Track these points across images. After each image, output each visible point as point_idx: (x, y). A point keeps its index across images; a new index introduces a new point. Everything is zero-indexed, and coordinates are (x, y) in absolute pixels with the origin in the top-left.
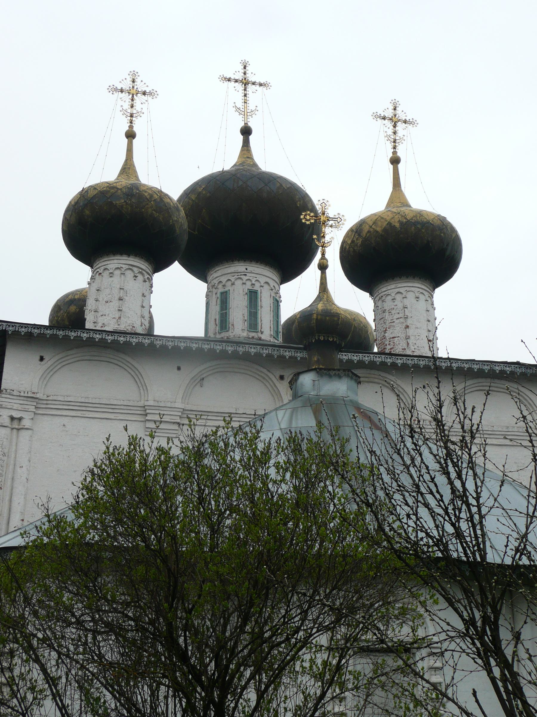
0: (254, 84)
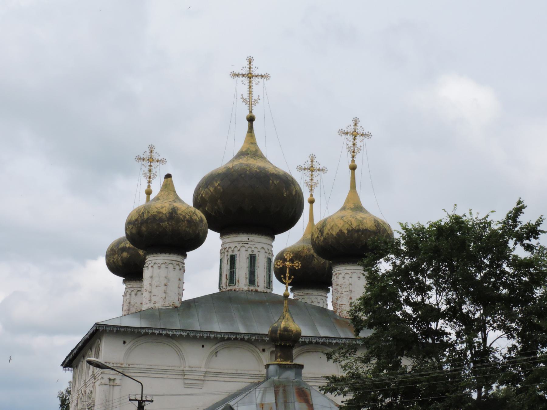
0: (257, 76)
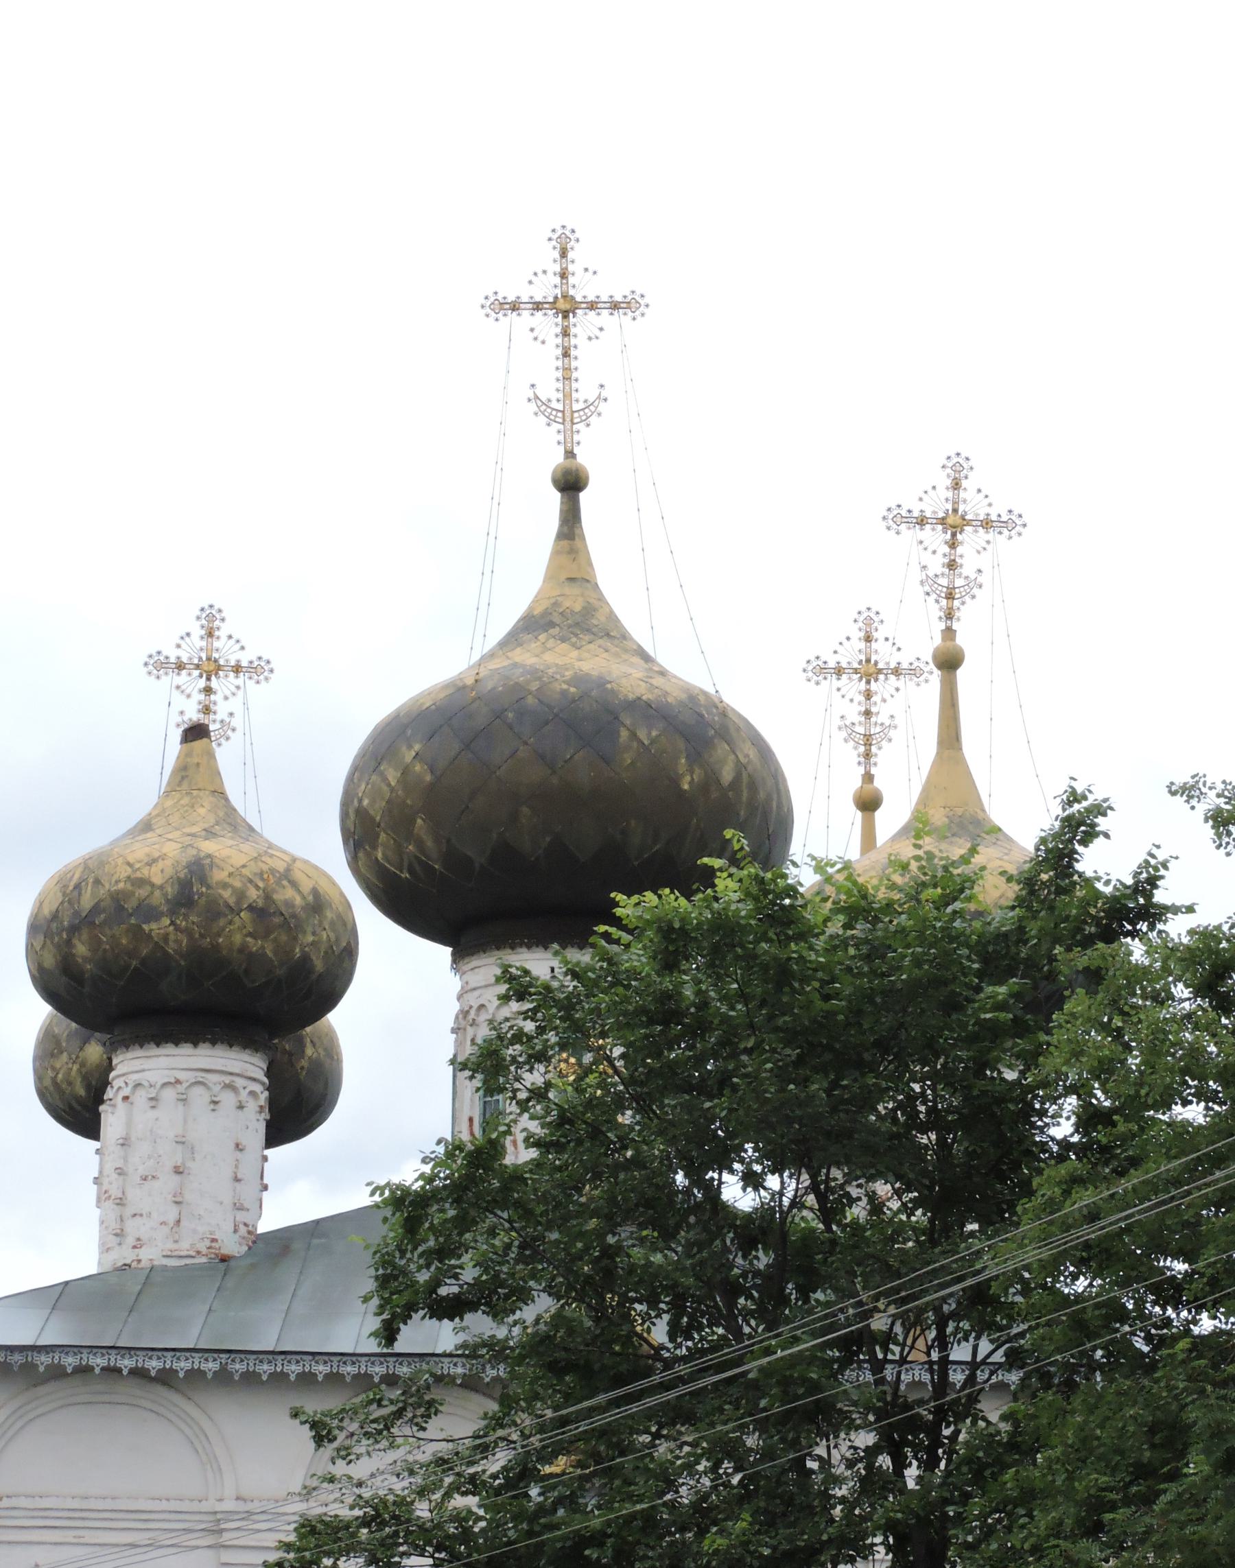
0: (592, 306)
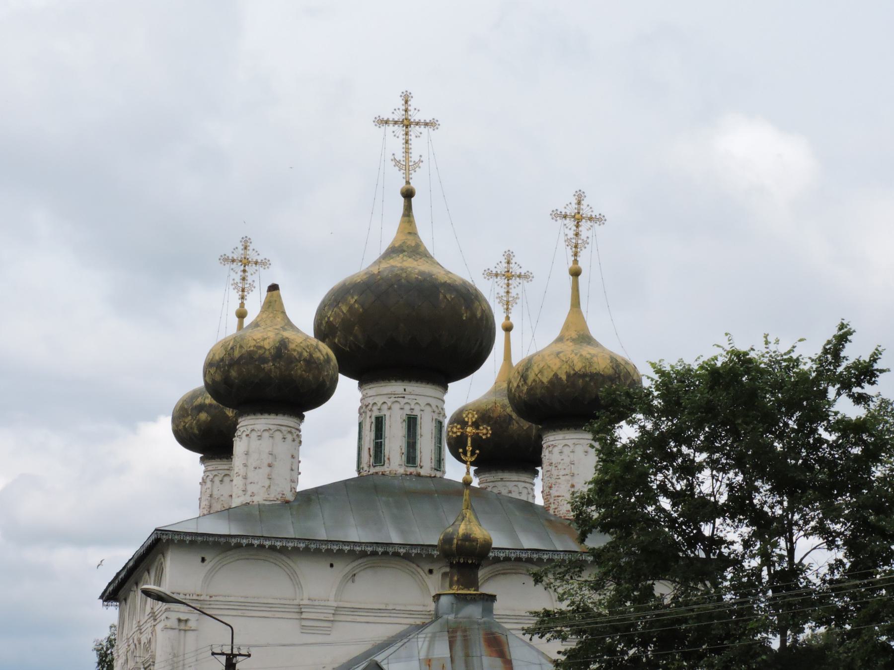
0: (417, 124)
